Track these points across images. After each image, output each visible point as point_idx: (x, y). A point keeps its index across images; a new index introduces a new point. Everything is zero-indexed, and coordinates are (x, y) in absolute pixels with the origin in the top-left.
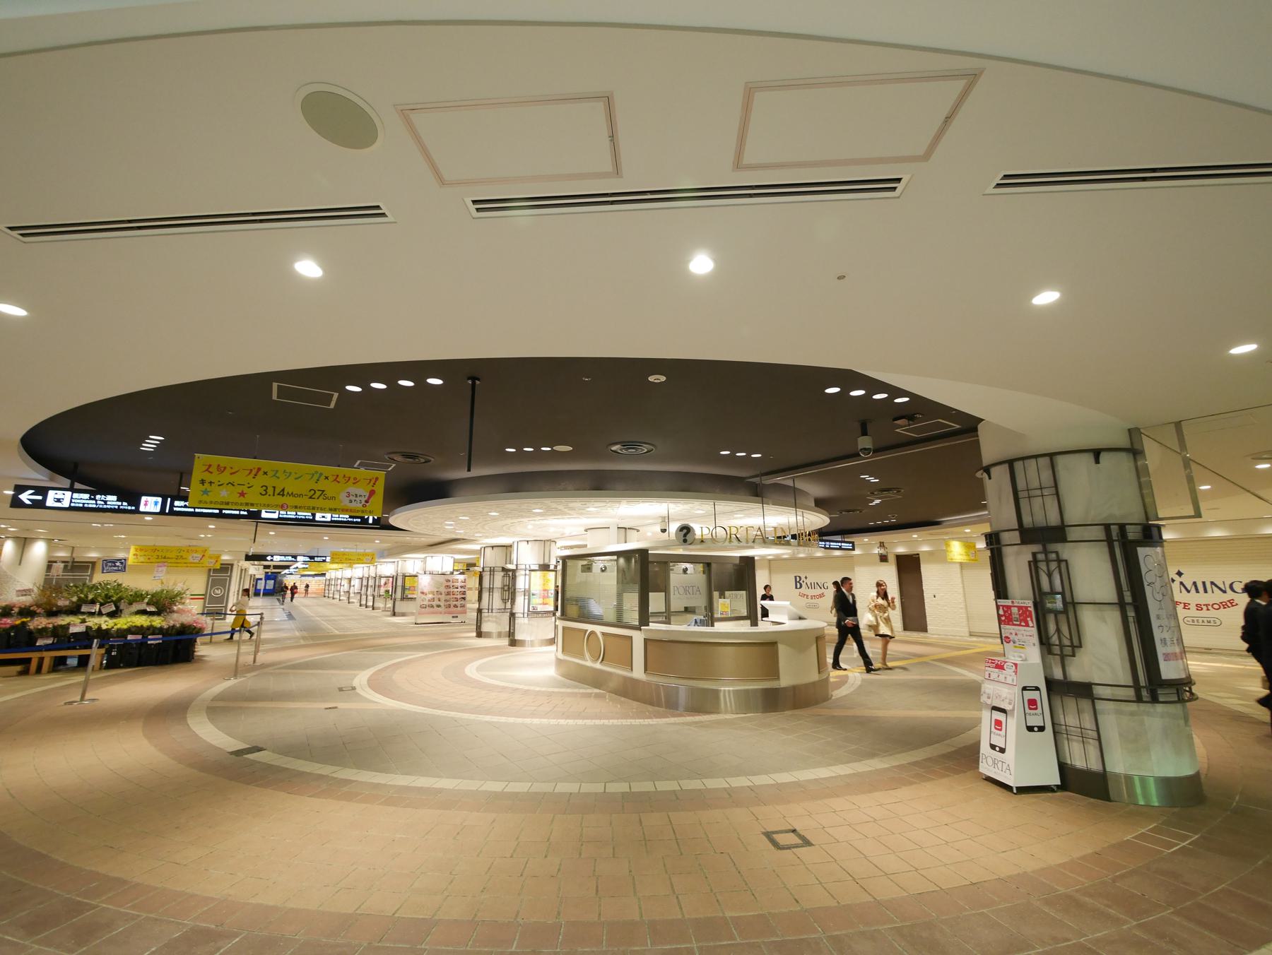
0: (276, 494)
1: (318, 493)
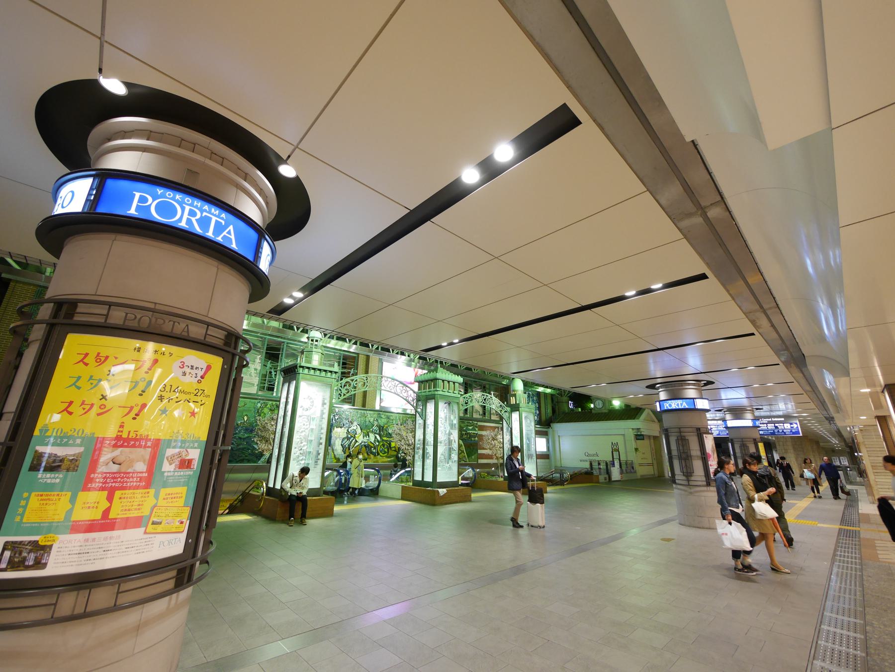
0: (171, 391)
1: (201, 392)
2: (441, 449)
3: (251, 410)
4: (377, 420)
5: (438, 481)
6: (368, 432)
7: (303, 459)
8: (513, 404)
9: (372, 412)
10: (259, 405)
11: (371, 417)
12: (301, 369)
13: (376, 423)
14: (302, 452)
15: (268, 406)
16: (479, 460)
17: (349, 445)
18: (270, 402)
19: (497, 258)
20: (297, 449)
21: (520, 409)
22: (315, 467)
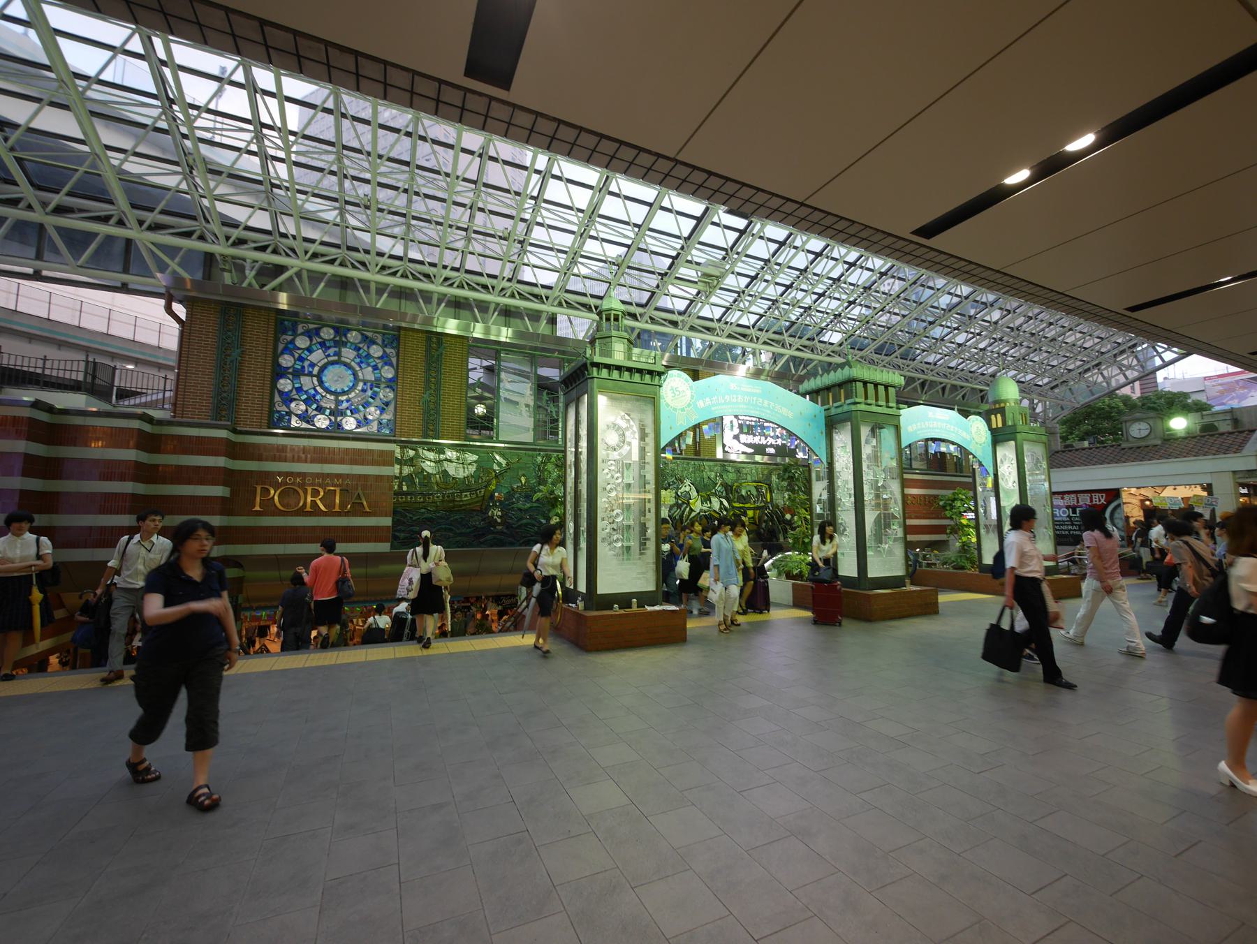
2: (870, 517)
3: (529, 468)
4: (721, 476)
5: (869, 576)
6: (708, 495)
7: (618, 539)
8: (997, 428)
9: (711, 463)
10: (539, 459)
11: (711, 471)
12: (595, 369)
13: (719, 482)
14: (615, 526)
15: (553, 459)
16: (908, 536)
17: (681, 516)
18: (555, 454)
19: (854, 235)
20: (606, 522)
21: (1019, 436)
22: (641, 554)
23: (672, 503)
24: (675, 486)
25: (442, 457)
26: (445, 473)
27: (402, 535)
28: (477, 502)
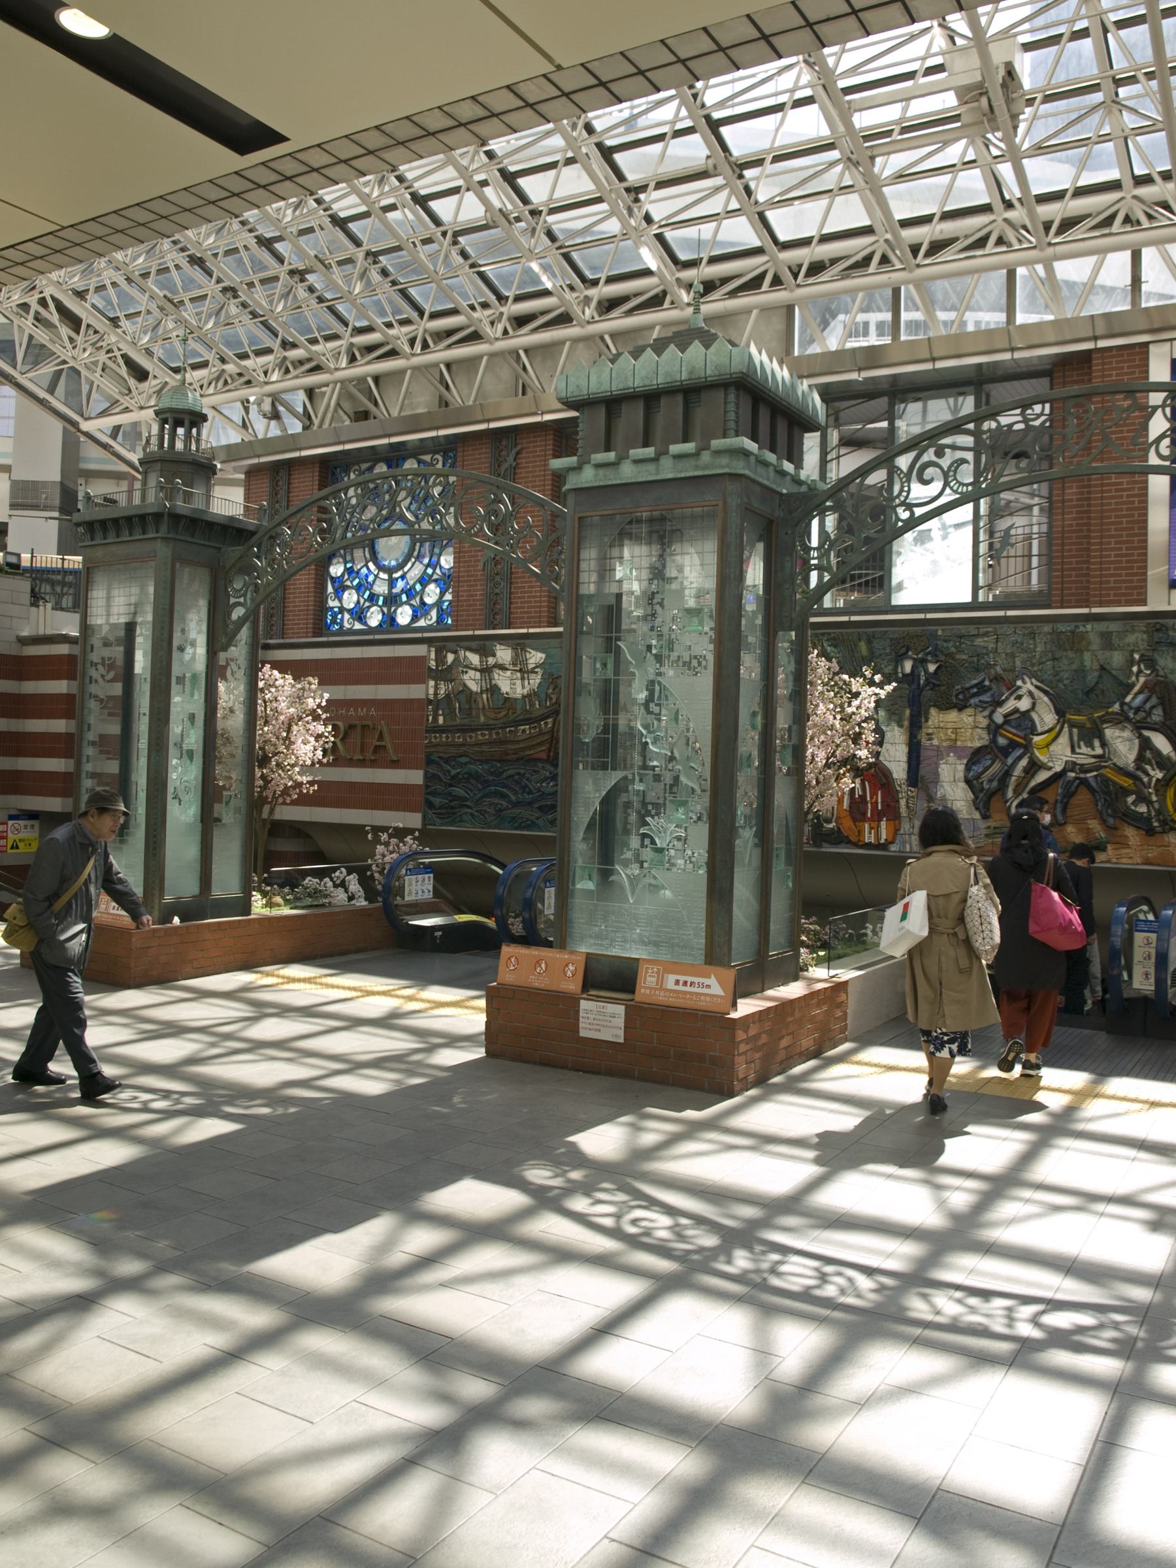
23: (978, 744)
24: (986, 698)
25: (491, 661)
26: (494, 690)
27: (437, 801)
28: (540, 744)
